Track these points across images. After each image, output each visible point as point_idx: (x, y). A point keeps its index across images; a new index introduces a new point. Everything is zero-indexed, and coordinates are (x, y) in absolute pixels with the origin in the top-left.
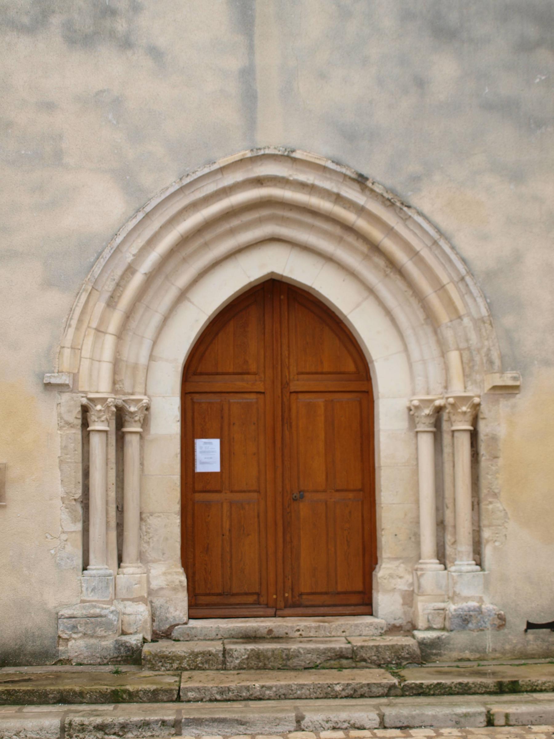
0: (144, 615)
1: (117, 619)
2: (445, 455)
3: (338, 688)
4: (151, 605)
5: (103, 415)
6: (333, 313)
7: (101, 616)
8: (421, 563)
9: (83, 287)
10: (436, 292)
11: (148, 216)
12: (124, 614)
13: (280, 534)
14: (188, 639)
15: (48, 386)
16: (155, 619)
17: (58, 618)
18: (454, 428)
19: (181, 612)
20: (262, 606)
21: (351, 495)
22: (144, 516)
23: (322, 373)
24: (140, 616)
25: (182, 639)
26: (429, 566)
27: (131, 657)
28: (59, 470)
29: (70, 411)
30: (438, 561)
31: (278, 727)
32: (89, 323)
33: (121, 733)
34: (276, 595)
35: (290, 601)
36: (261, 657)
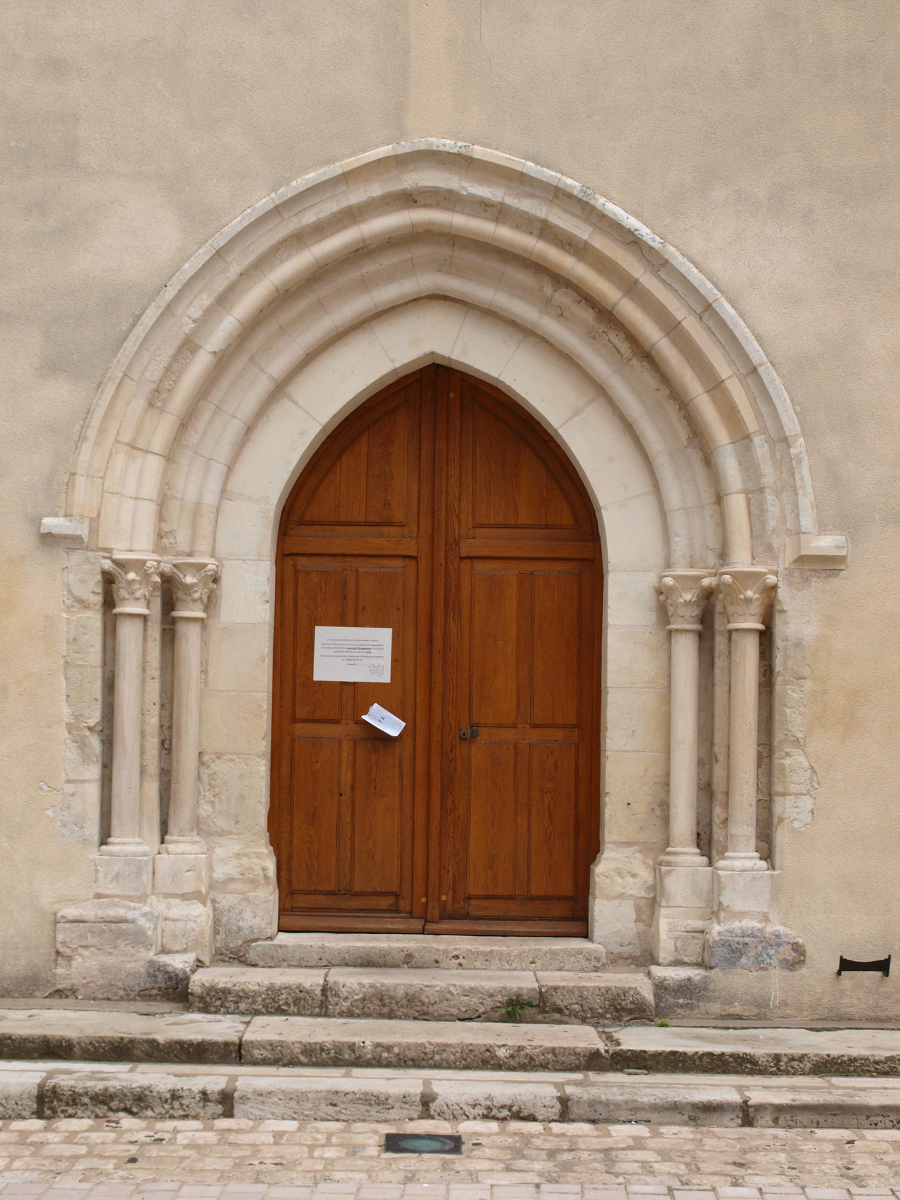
0: (199, 921)
1: (152, 926)
2: (717, 671)
3: (502, 1053)
4: (214, 906)
5: (139, 589)
6: (538, 423)
7: (126, 921)
8: (669, 854)
9: (109, 374)
10: (708, 391)
11: (219, 254)
12: (166, 919)
13: (436, 797)
14: (273, 964)
15: (49, 539)
16: (220, 929)
17: (56, 922)
18: (732, 626)
19: (263, 920)
20: (403, 915)
21: (558, 734)
22: (205, 758)
23: (516, 527)
24: (192, 923)
25: (262, 963)
26: (681, 858)
27: (175, 989)
28: (63, 678)
29: (83, 581)
30: (698, 851)
31: (391, 1111)
32: (118, 434)
33: (135, 1110)
34: (427, 897)
35: (449, 908)
36: (385, 997)
